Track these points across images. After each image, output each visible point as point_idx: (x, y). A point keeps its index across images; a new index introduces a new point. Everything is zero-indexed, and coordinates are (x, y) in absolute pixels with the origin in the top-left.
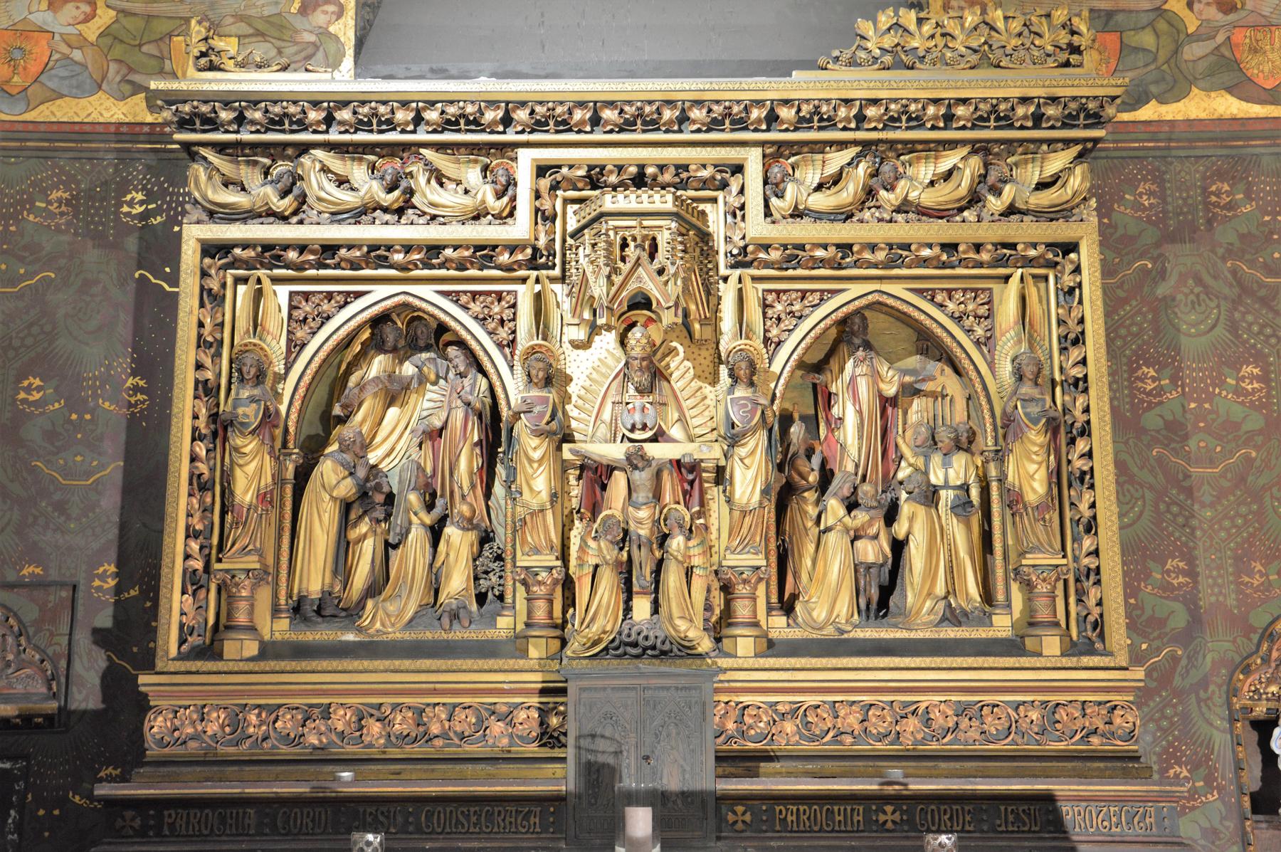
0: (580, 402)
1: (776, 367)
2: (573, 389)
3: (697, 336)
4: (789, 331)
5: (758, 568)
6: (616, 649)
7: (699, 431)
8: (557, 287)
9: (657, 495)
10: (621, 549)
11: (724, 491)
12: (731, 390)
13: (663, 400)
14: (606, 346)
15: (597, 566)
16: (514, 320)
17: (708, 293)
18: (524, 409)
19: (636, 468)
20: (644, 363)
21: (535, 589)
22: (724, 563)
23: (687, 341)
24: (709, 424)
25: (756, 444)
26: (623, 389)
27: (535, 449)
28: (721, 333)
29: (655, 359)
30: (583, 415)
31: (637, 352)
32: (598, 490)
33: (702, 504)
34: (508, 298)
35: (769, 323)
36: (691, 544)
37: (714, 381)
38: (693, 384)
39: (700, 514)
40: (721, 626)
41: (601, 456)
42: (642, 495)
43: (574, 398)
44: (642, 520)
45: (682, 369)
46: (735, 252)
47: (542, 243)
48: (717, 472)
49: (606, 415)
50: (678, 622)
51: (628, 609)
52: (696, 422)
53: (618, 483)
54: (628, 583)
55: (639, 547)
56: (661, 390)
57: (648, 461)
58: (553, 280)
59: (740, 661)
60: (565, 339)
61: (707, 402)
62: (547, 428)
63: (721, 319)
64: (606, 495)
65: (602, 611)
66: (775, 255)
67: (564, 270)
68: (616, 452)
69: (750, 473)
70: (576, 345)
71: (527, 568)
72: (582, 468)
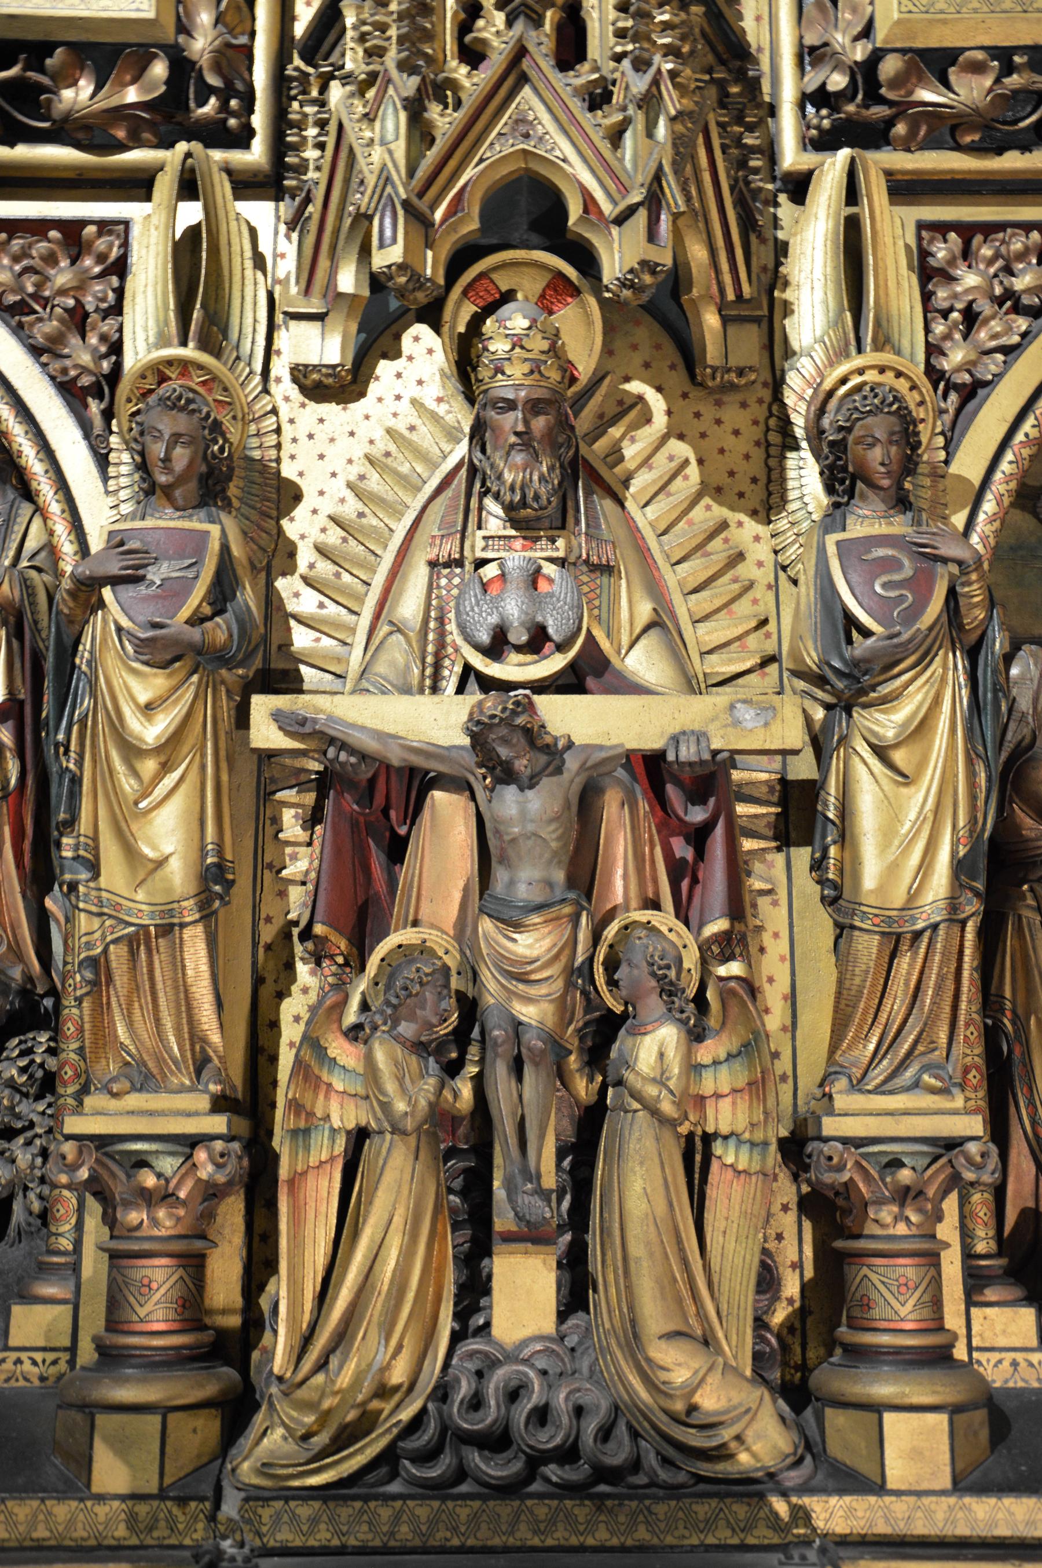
0: (325, 568)
1: (969, 463)
2: (301, 526)
3: (713, 354)
4: (1008, 350)
5: (952, 1144)
6: (428, 1456)
7: (721, 666)
8: (260, 213)
9: (583, 874)
10: (452, 1069)
11: (818, 865)
12: (835, 517)
13: (606, 554)
14: (411, 391)
15: (360, 1136)
16: (117, 309)
17: (748, 224)
18: (114, 568)
19: (505, 774)
20: (540, 423)
21: (134, 1217)
22: (830, 1126)
23: (678, 379)
24: (753, 641)
25: (928, 699)
26: (469, 516)
27: (149, 709)
28: (789, 353)
29: (583, 423)
30: (332, 609)
31: (513, 380)
32: (377, 860)
33: (737, 907)
34: (101, 244)
35: (939, 328)
36: (705, 1053)
37: (769, 499)
38: (698, 513)
39: (728, 946)
40: (811, 1348)
41: (380, 735)
42: (526, 879)
43: (305, 556)
44: (528, 966)
45: (662, 464)
46: (838, 81)
47: (201, 45)
48: (783, 802)
49: (410, 606)
50: (664, 1353)
51: (474, 1291)
52: (711, 633)
53: (446, 829)
54: (476, 1189)
55: (517, 1067)
56: (593, 523)
57: (551, 753)
58: (247, 185)
59: (899, 1507)
60: (280, 368)
61: (746, 570)
62: (195, 634)
63: (787, 309)
64: (403, 874)
65: (376, 1308)
66: (971, 90)
67: (279, 147)
68: (440, 722)
69: (917, 800)
70: (323, 387)
71: (102, 1141)
72: (324, 783)
